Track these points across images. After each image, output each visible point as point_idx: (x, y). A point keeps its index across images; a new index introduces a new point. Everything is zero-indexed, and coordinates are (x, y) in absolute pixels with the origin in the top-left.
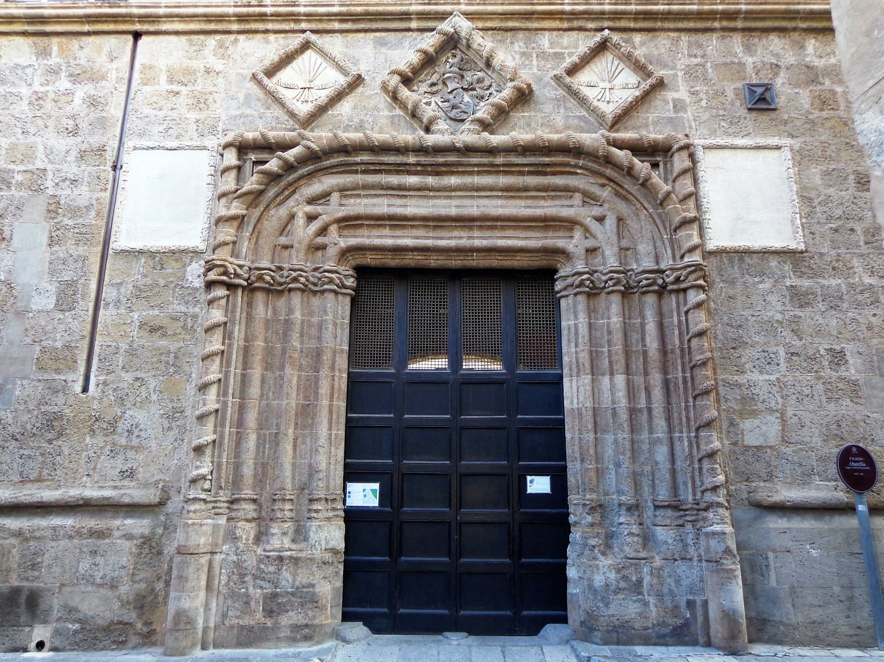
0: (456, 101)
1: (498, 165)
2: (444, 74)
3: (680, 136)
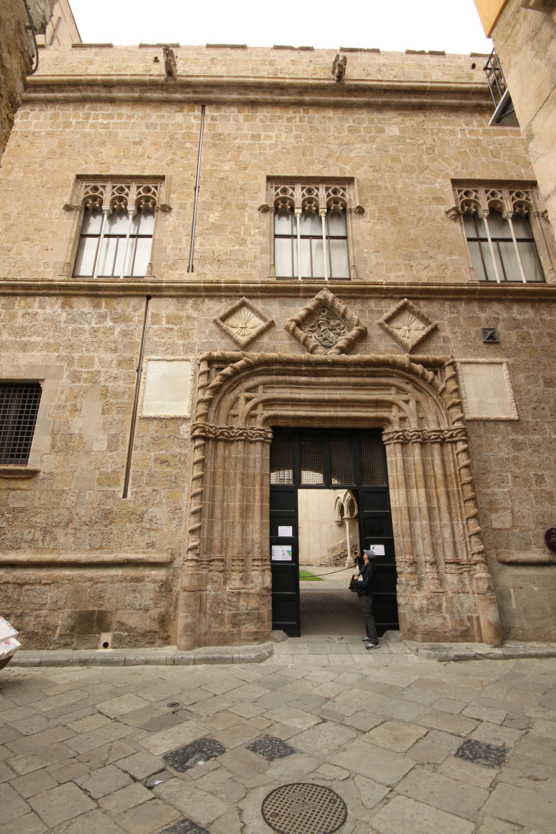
0: (326, 336)
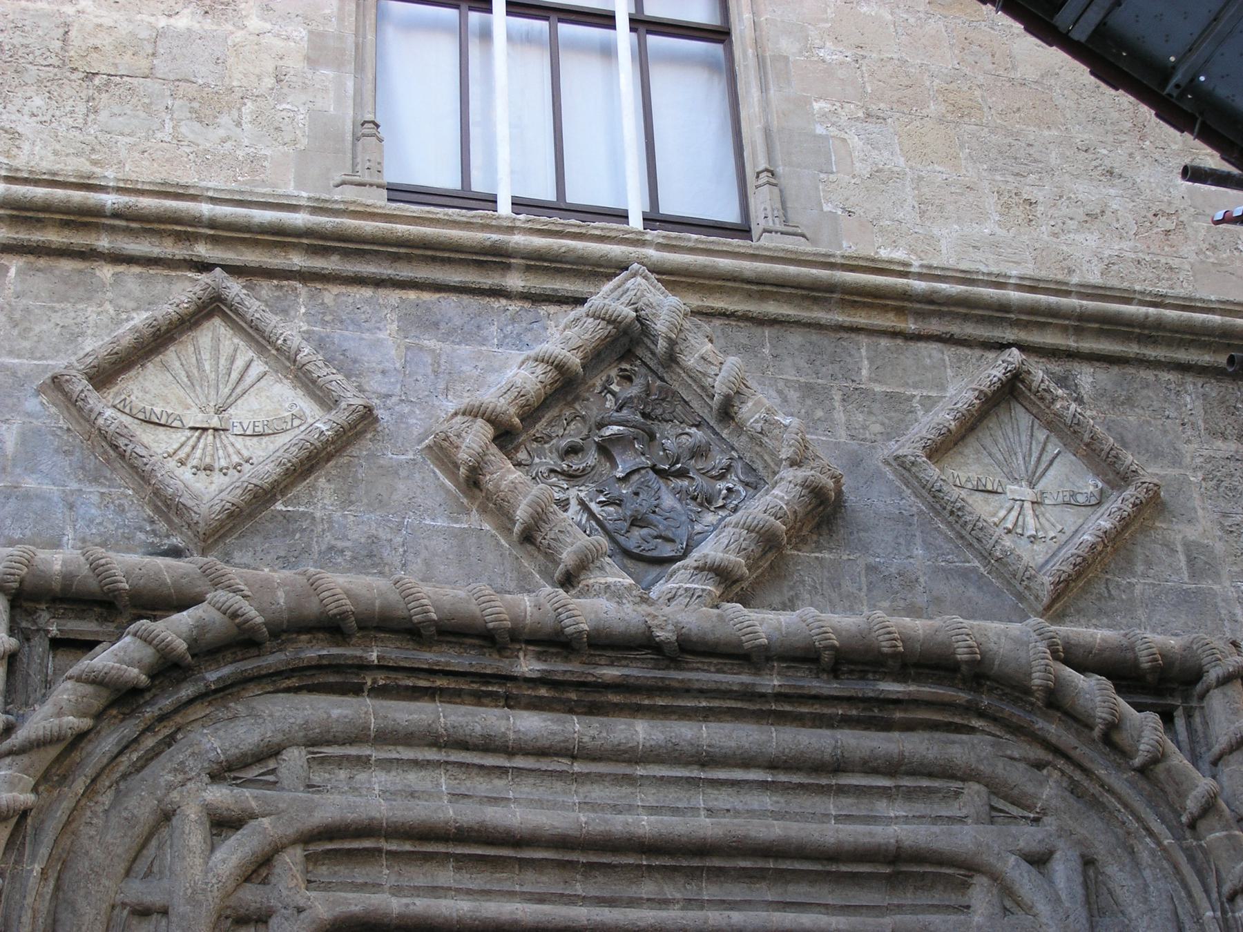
0: (643, 503)
1: (763, 696)
2: (601, 425)
3: (1218, 644)
